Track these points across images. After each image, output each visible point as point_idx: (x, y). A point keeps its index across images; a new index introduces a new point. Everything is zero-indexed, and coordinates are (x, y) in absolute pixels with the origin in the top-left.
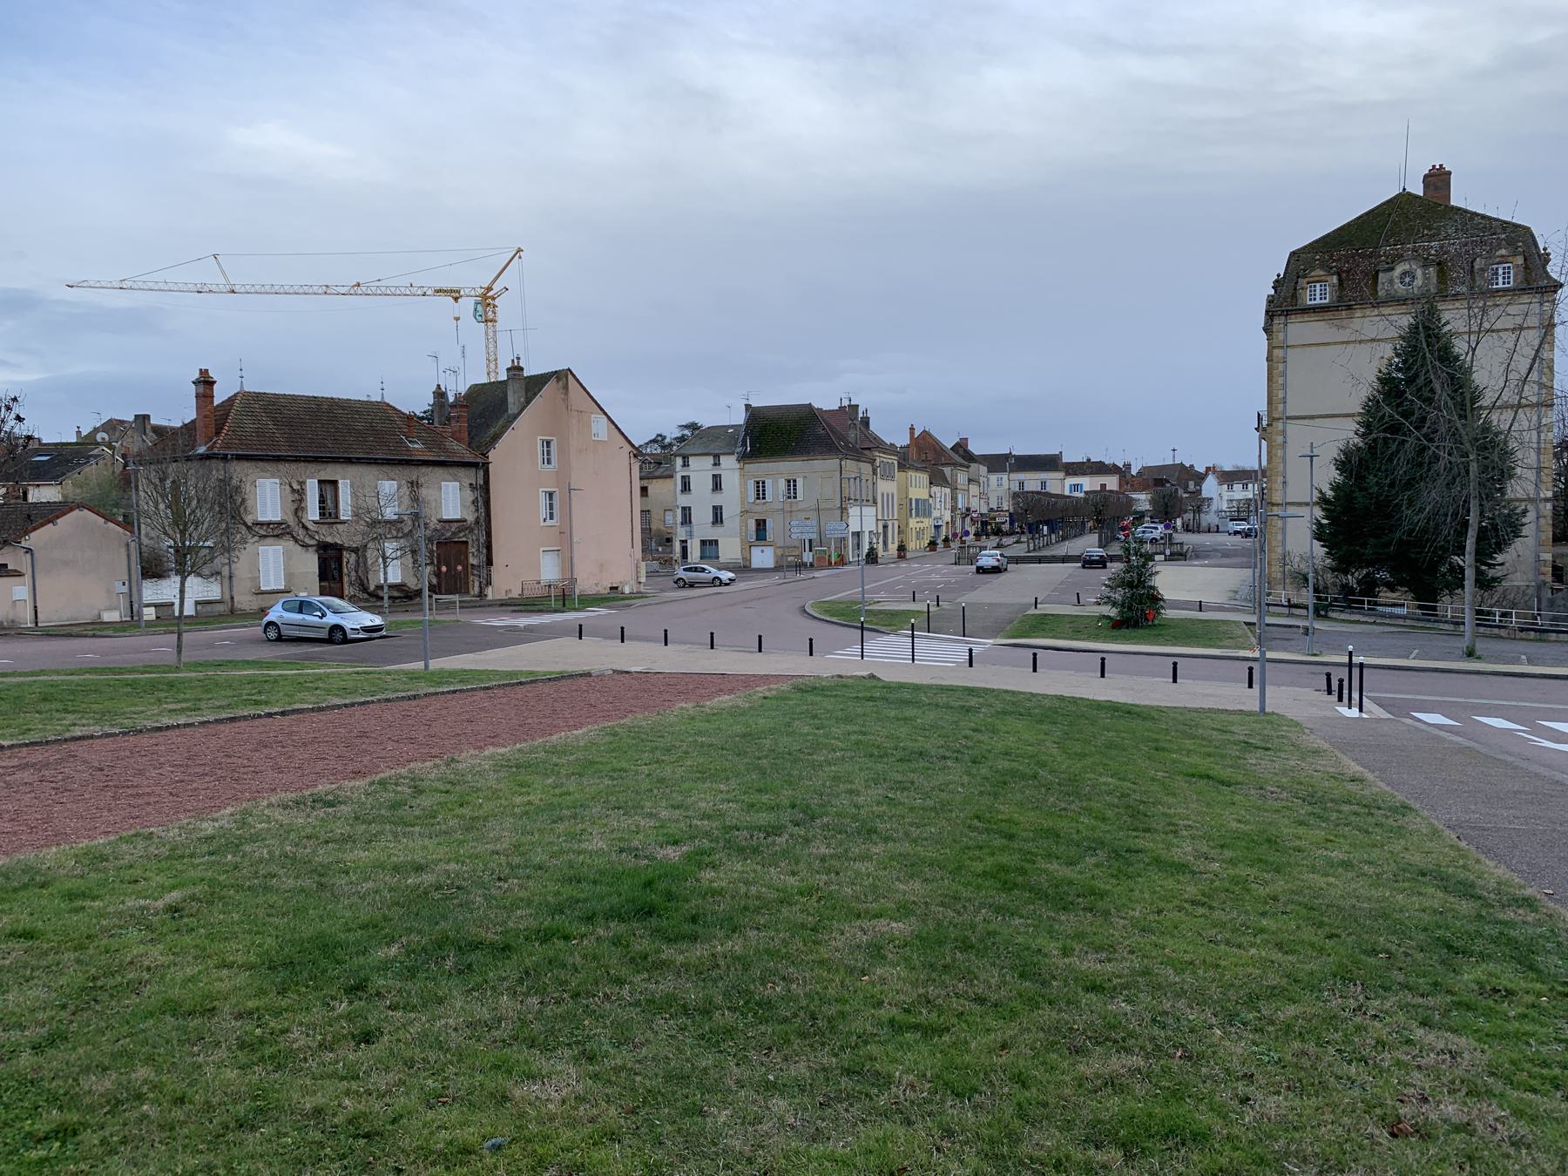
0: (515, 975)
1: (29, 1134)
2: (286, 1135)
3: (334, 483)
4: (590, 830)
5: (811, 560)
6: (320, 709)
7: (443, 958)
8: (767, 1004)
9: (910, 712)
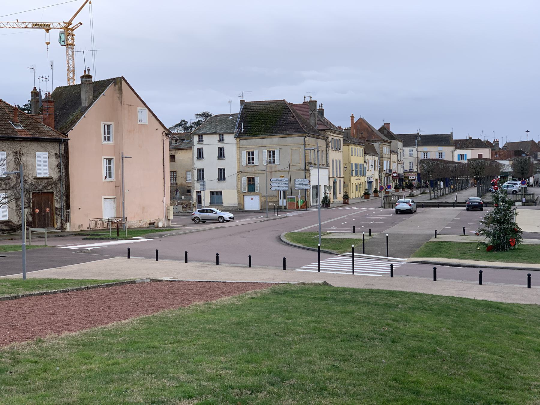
4: (132, 389)
5: (285, 205)
9: (350, 307)
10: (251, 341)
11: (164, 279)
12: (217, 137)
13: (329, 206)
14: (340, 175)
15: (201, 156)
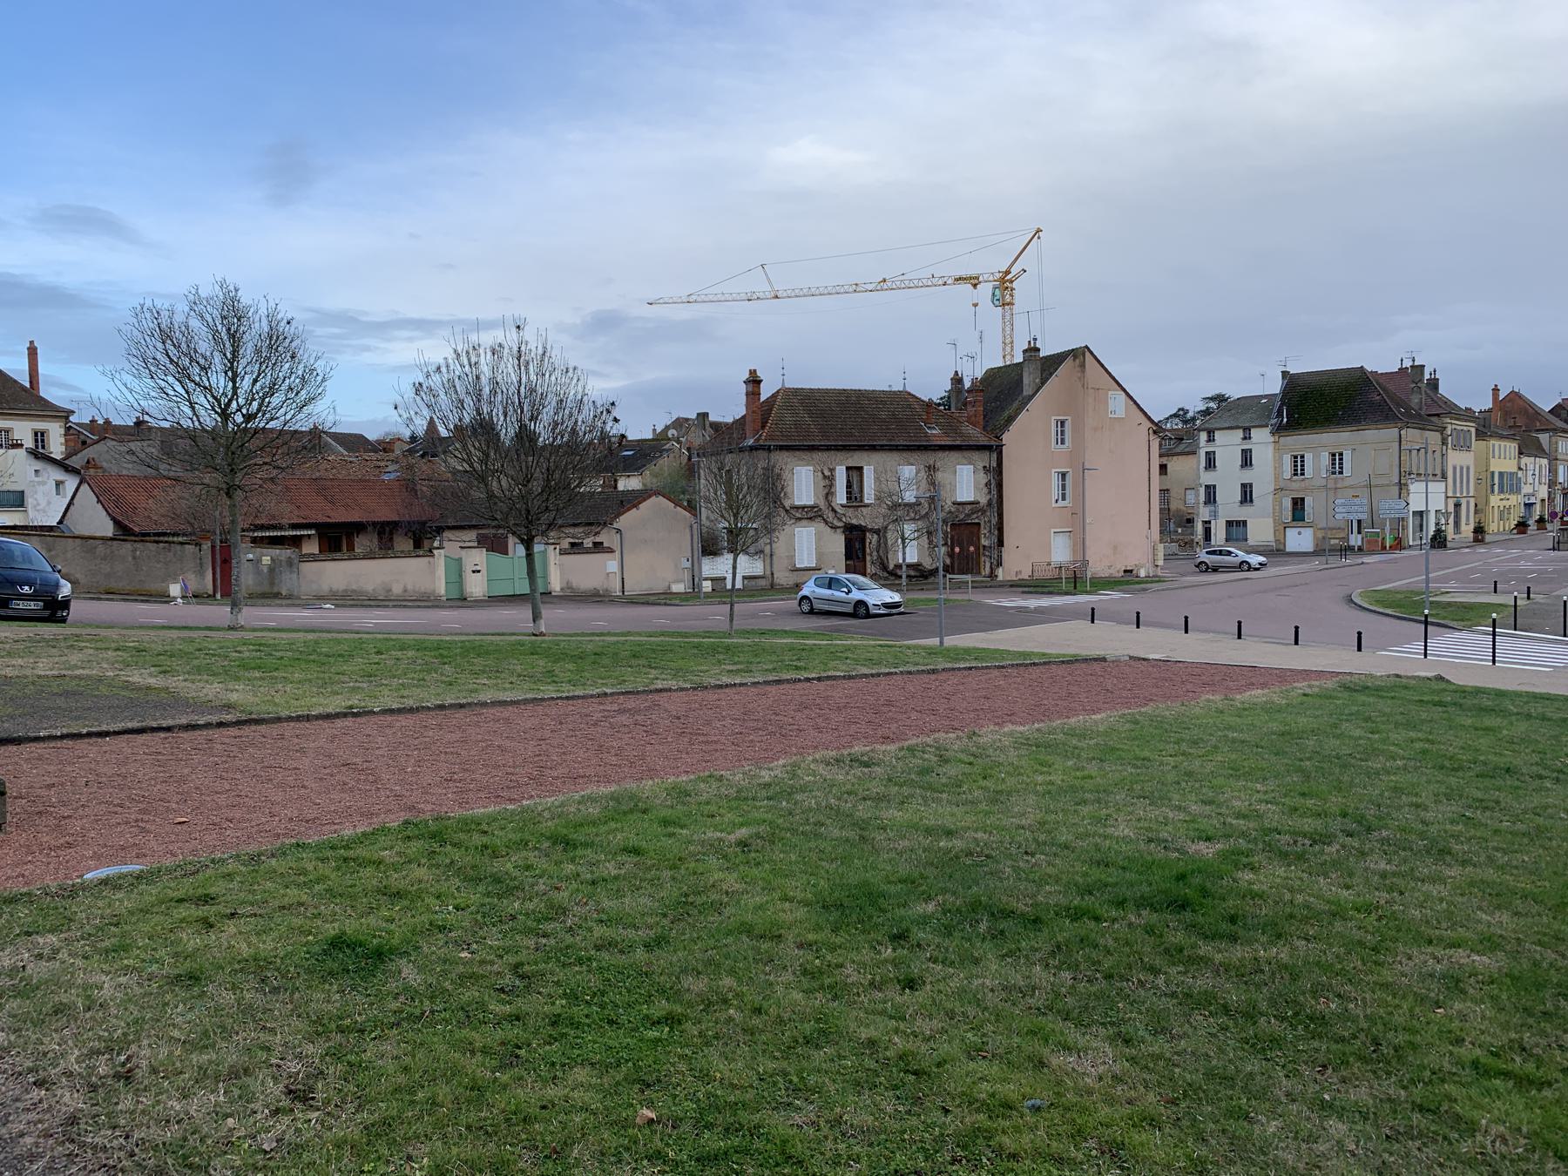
0: (1048, 948)
1: (647, 1017)
2: (845, 1058)
3: (860, 469)
4: (1115, 816)
5: (1360, 543)
6: (850, 677)
7: (977, 921)
8: (1321, 1019)
9: (1489, 721)
10: (1308, 763)
11: (1151, 656)
12: (1240, 433)
13: (1445, 546)
14: (1468, 492)
15: (1211, 463)
